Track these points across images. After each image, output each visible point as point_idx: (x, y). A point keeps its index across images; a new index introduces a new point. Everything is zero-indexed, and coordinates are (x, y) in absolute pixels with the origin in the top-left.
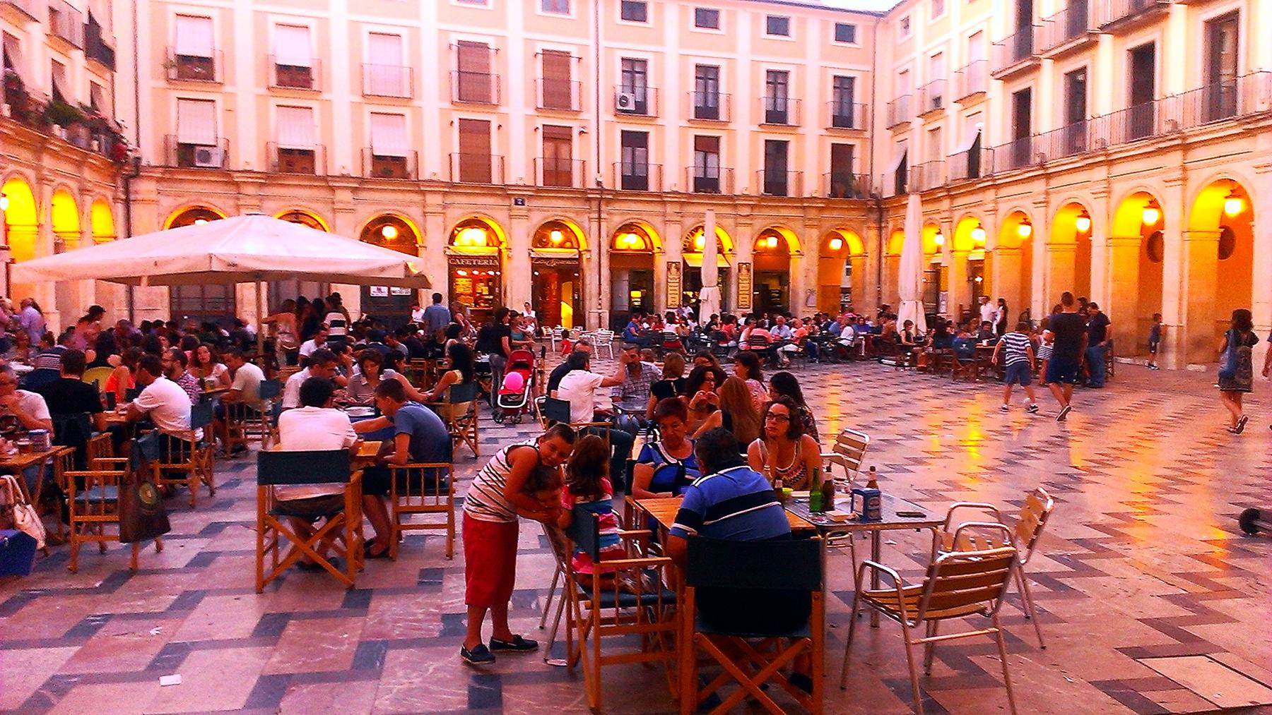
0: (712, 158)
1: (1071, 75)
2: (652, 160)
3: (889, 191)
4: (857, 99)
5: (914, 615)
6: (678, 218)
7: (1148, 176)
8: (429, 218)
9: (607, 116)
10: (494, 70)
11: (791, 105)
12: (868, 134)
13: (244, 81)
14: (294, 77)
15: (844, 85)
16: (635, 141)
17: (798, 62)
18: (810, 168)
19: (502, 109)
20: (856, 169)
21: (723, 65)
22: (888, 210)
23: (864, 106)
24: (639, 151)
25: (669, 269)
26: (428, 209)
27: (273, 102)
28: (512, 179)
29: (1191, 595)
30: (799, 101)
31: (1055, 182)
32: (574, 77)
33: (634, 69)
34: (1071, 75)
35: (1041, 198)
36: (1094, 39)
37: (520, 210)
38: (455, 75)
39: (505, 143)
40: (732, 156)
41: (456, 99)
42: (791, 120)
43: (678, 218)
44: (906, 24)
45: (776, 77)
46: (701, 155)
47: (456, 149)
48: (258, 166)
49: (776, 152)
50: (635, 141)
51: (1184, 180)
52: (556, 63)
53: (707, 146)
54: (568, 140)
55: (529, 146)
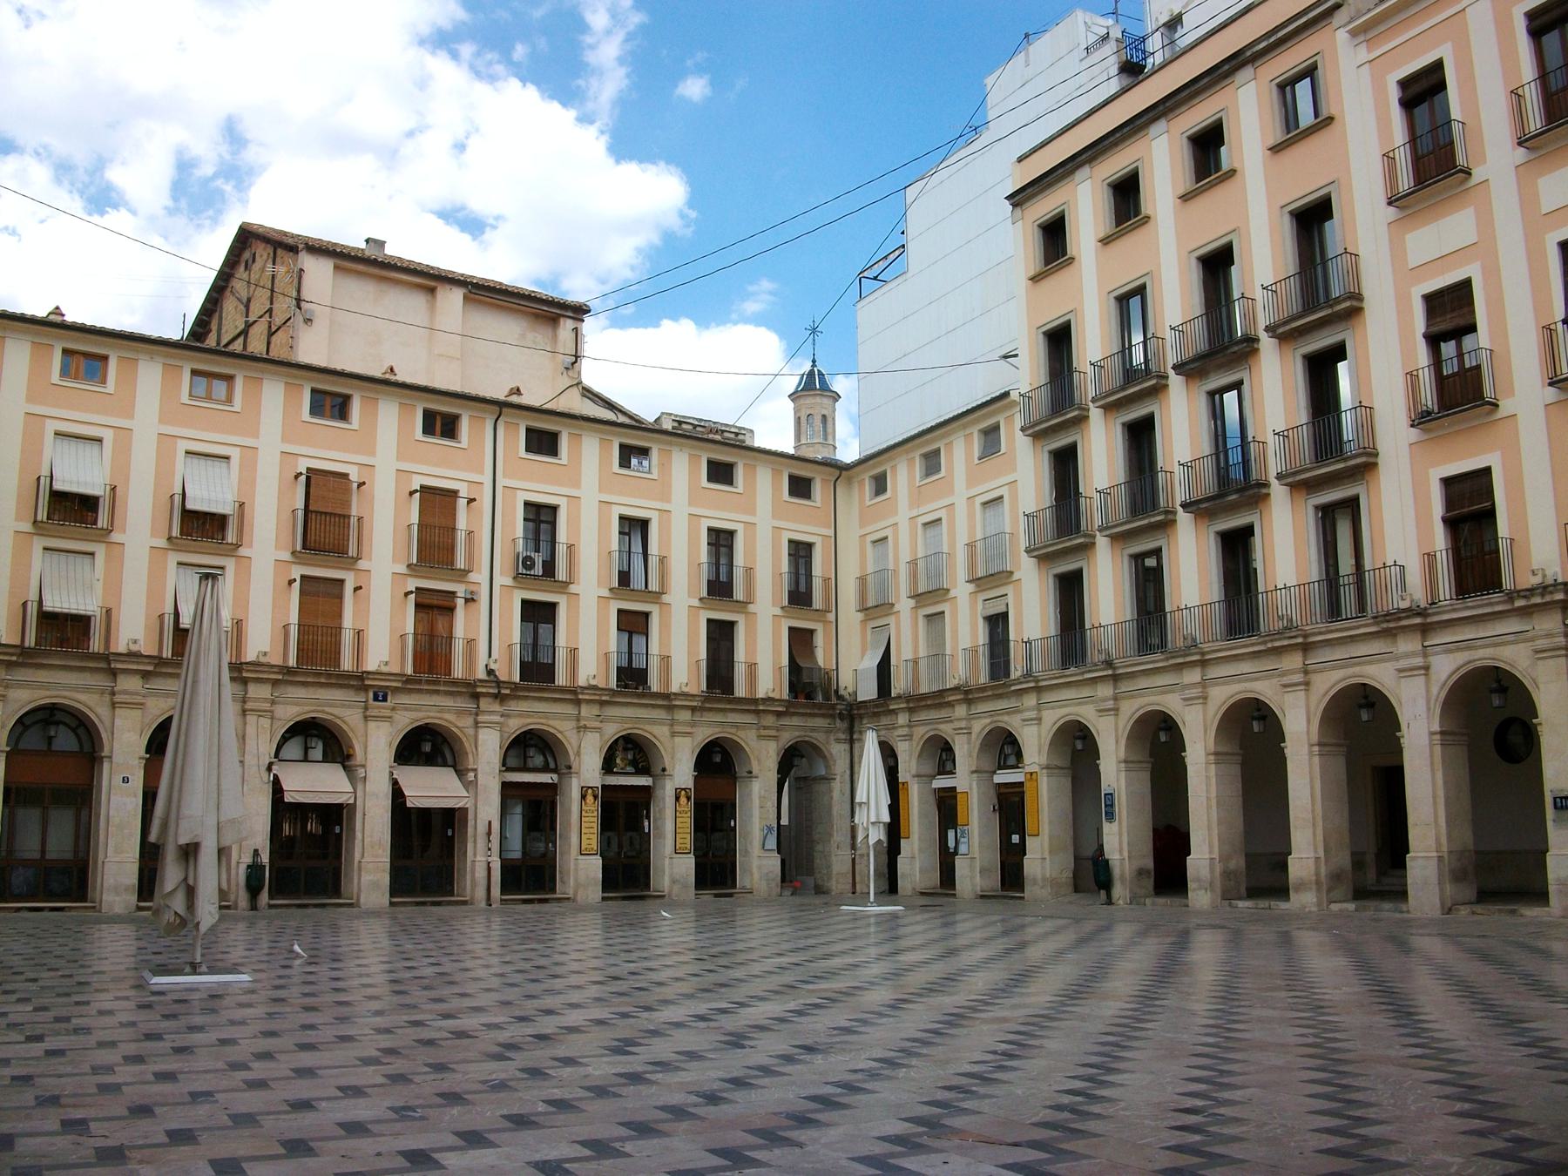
0: (638, 641)
1: (1138, 558)
2: (562, 640)
3: (868, 691)
4: (818, 569)
6: (597, 724)
7: (1257, 679)
8: (251, 719)
9: (503, 579)
10: (354, 512)
11: (738, 575)
12: (831, 617)
13: (140, 526)
14: (202, 527)
15: (801, 552)
16: (538, 615)
18: (763, 660)
19: (362, 564)
21: (654, 517)
22: (861, 717)
23: (826, 580)
24: (544, 628)
25: (677, 799)
26: (249, 706)
27: (173, 558)
28: (371, 664)
30: (570, 547)
31: (1124, 687)
32: (462, 522)
33: (541, 517)
34: (1138, 558)
35: (1110, 704)
36: (1170, 517)
37: (377, 708)
38: (300, 514)
39: (363, 611)
40: (665, 642)
41: (299, 548)
42: (739, 593)
43: (597, 724)
44: (880, 485)
45: (538, 514)
46: (626, 636)
47: (294, 618)
48: (147, 648)
49: (721, 636)
50: (538, 615)
51: (1307, 684)
52: (437, 503)
53: (633, 624)
54: (450, 610)
55: (279, 605)
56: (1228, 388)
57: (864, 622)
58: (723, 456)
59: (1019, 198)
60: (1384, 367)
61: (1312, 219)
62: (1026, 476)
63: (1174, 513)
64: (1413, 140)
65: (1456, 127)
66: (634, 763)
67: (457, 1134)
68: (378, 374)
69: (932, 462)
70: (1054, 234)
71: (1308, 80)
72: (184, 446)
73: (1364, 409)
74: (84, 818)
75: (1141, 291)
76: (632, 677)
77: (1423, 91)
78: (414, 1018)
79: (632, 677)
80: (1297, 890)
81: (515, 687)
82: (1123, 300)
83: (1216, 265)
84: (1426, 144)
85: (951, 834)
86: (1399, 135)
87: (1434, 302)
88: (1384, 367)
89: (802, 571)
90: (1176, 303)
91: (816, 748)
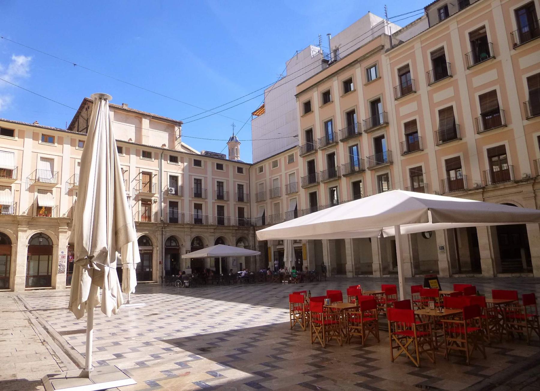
4: (245, 192)
5: (503, 335)
15: (240, 187)
17: (226, 179)
20: (246, 216)
23: (247, 194)
24: (199, 211)
29: (373, 371)
42: (225, 198)
44: (261, 170)
49: (221, 209)
53: (198, 207)
56: (354, 146)
57: (257, 205)
58: (220, 162)
59: (297, 96)
60: (395, 139)
61: (374, 104)
62: (301, 168)
63: (341, 177)
64: (401, 84)
65: (412, 81)
66: (199, 244)
67: (114, 355)
68: (127, 141)
69: (275, 164)
70: (307, 107)
71: (401, 115)
72: (40, 155)
73: (390, 152)
74: (50, 259)
75: (331, 121)
76: (198, 221)
77: (404, 72)
78: (120, 320)
79: (198, 221)
80: (375, 271)
81: (168, 225)
82: (326, 124)
83: (350, 115)
84: (404, 85)
85: (99, 291)
86: (397, 83)
87: (407, 125)
88: (395, 139)
89: (199, 187)
90: (340, 124)
91: (245, 238)
